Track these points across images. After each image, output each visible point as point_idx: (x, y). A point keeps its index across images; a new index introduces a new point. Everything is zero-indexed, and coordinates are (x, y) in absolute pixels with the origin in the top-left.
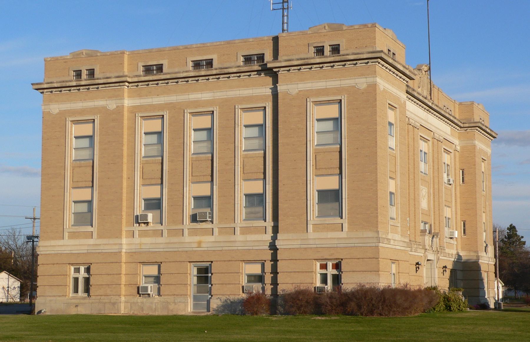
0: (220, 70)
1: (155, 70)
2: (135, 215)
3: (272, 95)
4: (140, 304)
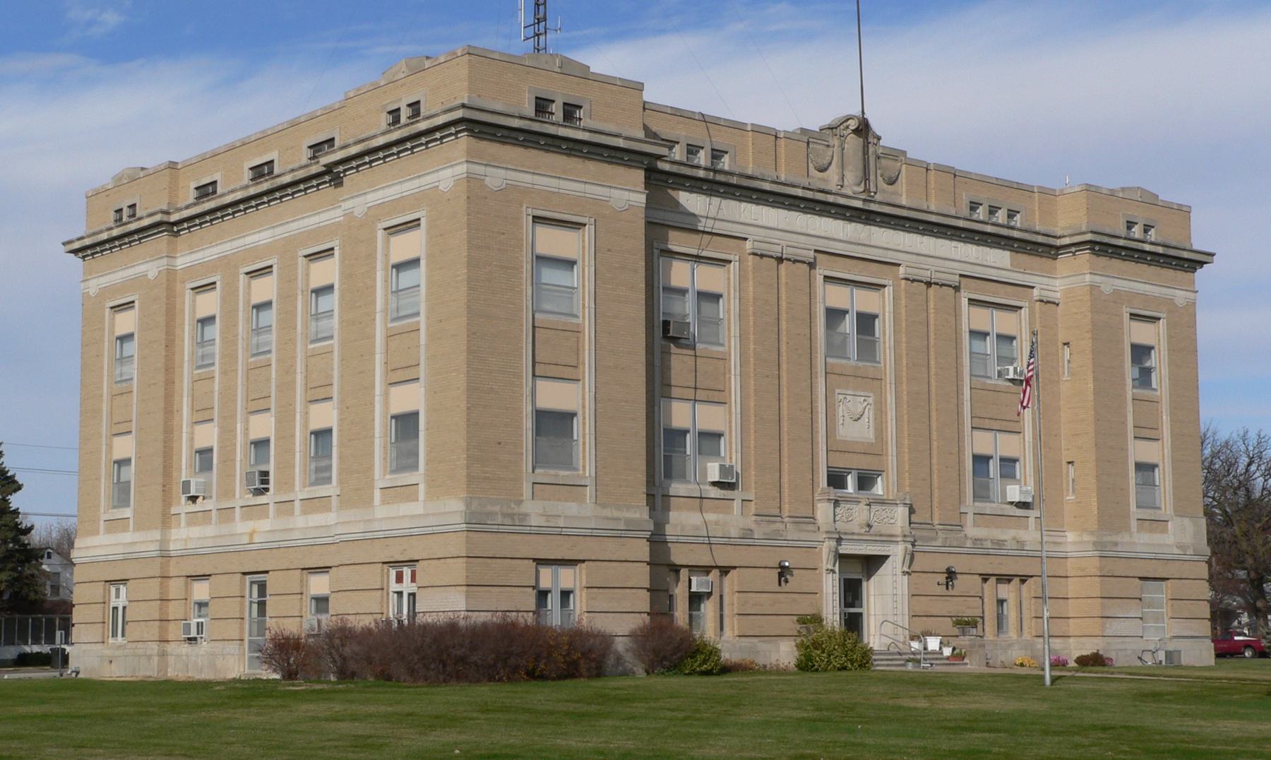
4: (184, 658)
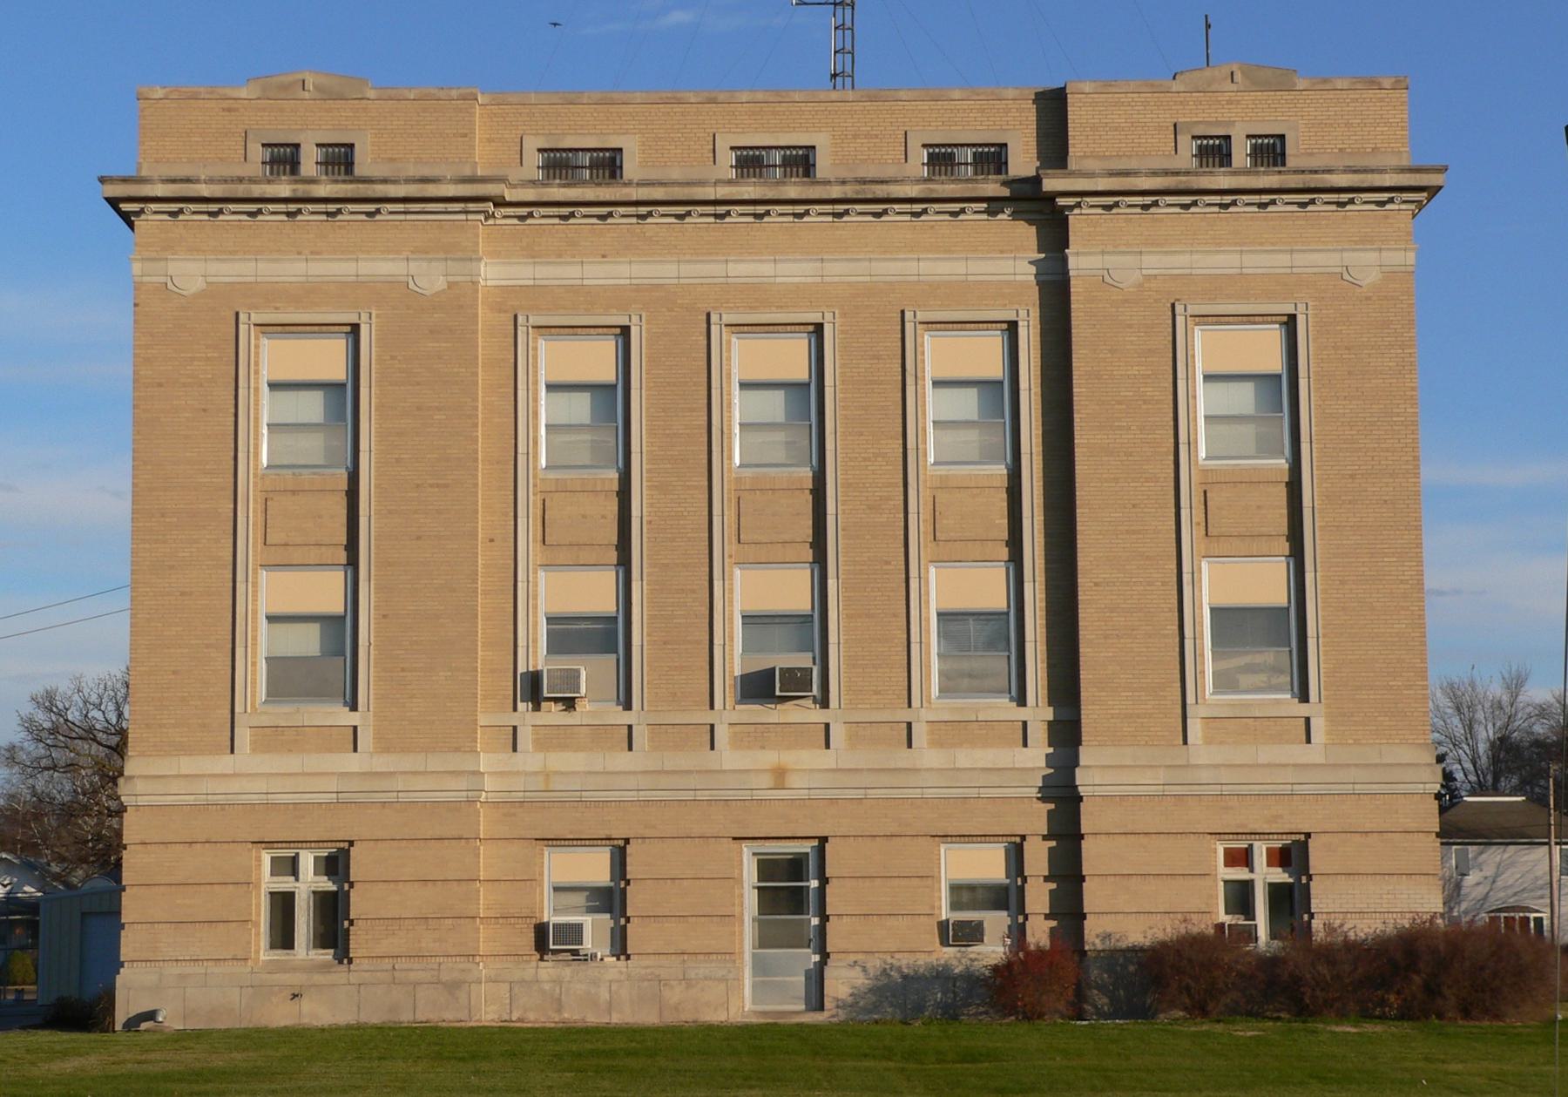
0: (858, 187)
1: (779, 166)
2: (521, 669)
3: (1037, 284)
4: (547, 987)
